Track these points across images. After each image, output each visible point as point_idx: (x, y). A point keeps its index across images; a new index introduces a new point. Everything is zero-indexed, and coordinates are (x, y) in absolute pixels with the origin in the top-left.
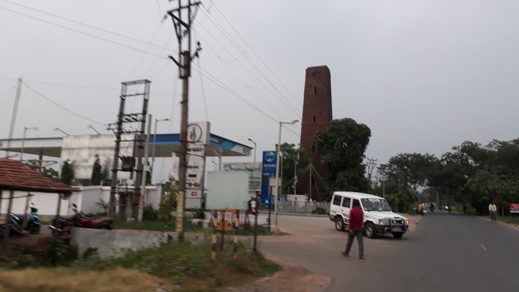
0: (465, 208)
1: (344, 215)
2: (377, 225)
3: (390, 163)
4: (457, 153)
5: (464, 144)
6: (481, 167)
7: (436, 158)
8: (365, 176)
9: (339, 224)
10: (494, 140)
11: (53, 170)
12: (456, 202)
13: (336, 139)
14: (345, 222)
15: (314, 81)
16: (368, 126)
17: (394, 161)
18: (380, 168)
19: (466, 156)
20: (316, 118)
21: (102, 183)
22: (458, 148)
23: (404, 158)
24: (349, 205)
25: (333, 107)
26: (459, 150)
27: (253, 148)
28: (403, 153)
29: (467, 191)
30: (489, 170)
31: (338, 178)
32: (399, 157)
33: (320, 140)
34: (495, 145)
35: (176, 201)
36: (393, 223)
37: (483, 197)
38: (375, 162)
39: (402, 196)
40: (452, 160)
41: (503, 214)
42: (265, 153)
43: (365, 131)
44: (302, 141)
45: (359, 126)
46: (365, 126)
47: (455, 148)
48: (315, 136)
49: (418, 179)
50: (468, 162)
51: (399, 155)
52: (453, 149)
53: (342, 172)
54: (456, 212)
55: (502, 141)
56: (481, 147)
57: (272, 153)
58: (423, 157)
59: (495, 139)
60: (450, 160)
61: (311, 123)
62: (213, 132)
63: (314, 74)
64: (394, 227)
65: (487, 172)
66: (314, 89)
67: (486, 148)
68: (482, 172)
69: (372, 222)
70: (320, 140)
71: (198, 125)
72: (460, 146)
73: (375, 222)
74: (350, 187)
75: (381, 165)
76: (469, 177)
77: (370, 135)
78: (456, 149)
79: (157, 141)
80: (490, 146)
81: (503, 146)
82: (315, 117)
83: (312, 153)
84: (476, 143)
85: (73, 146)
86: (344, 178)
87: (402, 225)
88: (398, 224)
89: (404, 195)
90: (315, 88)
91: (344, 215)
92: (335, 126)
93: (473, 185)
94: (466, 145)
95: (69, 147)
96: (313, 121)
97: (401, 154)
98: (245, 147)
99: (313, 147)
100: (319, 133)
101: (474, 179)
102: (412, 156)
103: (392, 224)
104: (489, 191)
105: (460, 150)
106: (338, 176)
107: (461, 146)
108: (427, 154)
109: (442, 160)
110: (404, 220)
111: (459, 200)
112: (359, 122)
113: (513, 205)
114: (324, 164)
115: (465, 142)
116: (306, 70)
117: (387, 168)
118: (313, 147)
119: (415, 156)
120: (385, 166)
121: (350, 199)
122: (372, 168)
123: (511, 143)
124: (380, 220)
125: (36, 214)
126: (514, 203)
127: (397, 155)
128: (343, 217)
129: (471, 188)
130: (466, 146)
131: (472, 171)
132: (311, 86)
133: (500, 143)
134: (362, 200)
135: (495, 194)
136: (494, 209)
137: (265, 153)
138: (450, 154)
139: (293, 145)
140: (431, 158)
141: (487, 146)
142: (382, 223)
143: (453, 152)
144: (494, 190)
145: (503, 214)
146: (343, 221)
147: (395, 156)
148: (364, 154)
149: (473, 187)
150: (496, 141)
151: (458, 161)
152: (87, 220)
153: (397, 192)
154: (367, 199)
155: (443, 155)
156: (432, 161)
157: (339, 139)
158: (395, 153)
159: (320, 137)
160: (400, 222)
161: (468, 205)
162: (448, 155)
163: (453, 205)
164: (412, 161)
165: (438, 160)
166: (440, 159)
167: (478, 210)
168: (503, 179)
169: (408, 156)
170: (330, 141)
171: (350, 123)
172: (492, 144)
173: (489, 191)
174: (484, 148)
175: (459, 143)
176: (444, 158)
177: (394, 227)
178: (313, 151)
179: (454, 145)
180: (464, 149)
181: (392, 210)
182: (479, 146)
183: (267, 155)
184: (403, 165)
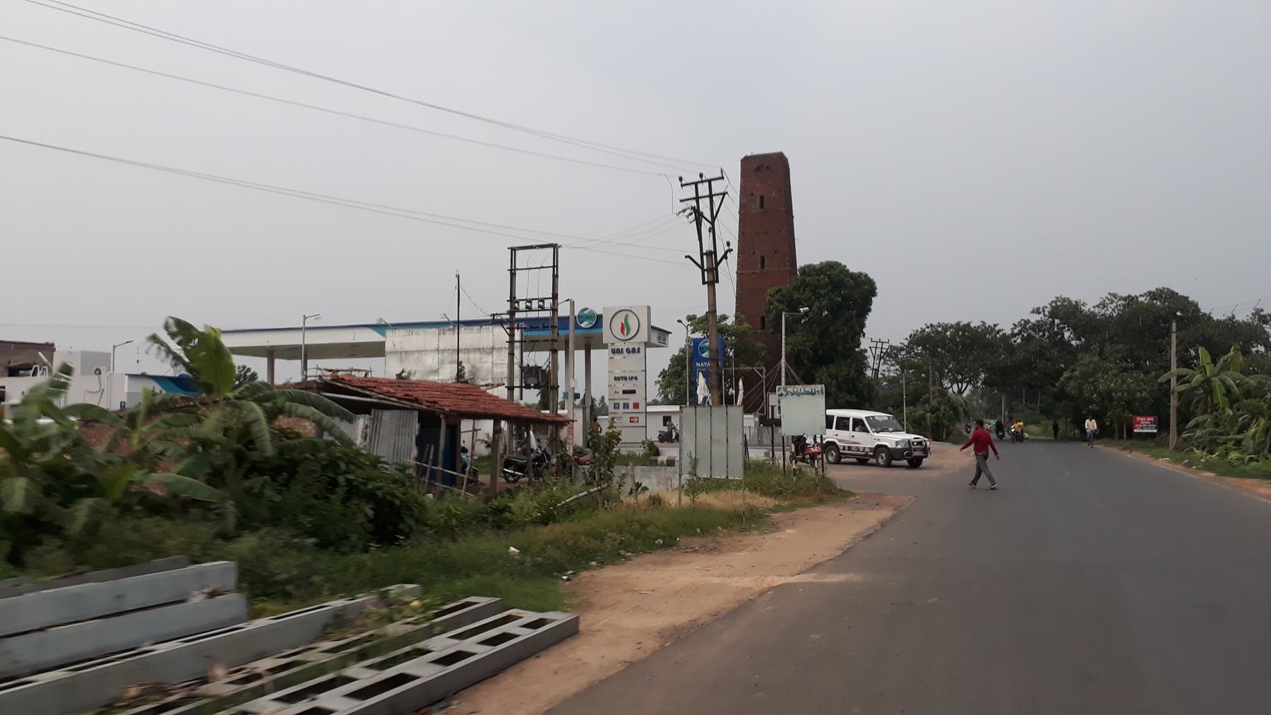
0: (1056, 428)
1: (840, 441)
2: (894, 449)
4: (1042, 321)
5: (1055, 302)
6: (1085, 348)
7: (1000, 331)
9: (832, 455)
10: (1110, 294)
12: (1043, 416)
14: (841, 451)
16: (871, 276)
19: (1058, 325)
24: (848, 426)
26: (1044, 314)
27: (671, 333)
28: (935, 323)
29: (1062, 395)
30: (1100, 355)
32: (927, 330)
34: (1112, 303)
35: (43, 435)
36: (914, 445)
39: (938, 409)
40: (1033, 333)
41: (1125, 436)
43: (866, 287)
44: (739, 308)
45: (852, 276)
46: (866, 276)
47: (1037, 311)
49: (963, 373)
50: (1063, 336)
52: (1033, 312)
54: (1043, 437)
55: (1125, 295)
56: (1085, 309)
58: (977, 328)
59: (1111, 292)
60: (1029, 334)
61: (757, 271)
62: (652, 324)
63: (758, 169)
64: (915, 450)
65: (1096, 359)
66: (758, 199)
67: (1097, 310)
68: (1087, 359)
69: (886, 446)
71: (616, 313)
72: (1046, 307)
73: (889, 446)
74: (841, 395)
77: (874, 294)
78: (1039, 313)
80: (1103, 305)
81: (1128, 304)
82: (763, 258)
83: (760, 331)
84: (1075, 302)
85: (407, 348)
87: (923, 447)
88: (919, 446)
90: (762, 198)
91: (840, 441)
92: (807, 279)
93: (1072, 383)
95: (398, 348)
97: (931, 325)
98: (661, 333)
99: (763, 319)
100: (777, 292)
103: (913, 447)
104: (1099, 394)
105: (1047, 313)
106: (817, 375)
107: (1049, 306)
108: (983, 322)
109: (1014, 335)
110: (925, 441)
111: (1047, 412)
112: (853, 268)
113: (1138, 419)
114: (790, 353)
115: (1056, 299)
116: (742, 161)
117: (903, 353)
118: (763, 319)
119: (958, 327)
121: (849, 419)
123: (1141, 299)
124: (897, 443)
125: (471, 447)
126: (1141, 415)
127: (924, 327)
128: (838, 443)
129: (1068, 390)
133: (1121, 298)
134: (867, 418)
135: (1111, 399)
136: (1094, 427)
138: (1028, 322)
140: (991, 330)
141: (1098, 306)
142: (899, 447)
143: (1034, 318)
144: (1109, 392)
145: (1125, 436)
146: (839, 449)
147: (920, 330)
149: (1071, 388)
150: (1115, 296)
151: (1044, 335)
152: (909, 426)
153: (927, 401)
154: (873, 417)
155: (1014, 325)
156: (992, 338)
160: (920, 443)
163: (1036, 423)
164: (953, 339)
165: (1004, 334)
166: (1008, 332)
168: (1125, 370)
169: (946, 328)
171: (836, 272)
172: (1107, 302)
173: (1099, 394)
174: (1092, 309)
175: (1045, 301)
176: (1016, 331)
177: (915, 450)
178: (763, 327)
179: (1036, 306)
180: (1054, 312)
182: (1083, 308)
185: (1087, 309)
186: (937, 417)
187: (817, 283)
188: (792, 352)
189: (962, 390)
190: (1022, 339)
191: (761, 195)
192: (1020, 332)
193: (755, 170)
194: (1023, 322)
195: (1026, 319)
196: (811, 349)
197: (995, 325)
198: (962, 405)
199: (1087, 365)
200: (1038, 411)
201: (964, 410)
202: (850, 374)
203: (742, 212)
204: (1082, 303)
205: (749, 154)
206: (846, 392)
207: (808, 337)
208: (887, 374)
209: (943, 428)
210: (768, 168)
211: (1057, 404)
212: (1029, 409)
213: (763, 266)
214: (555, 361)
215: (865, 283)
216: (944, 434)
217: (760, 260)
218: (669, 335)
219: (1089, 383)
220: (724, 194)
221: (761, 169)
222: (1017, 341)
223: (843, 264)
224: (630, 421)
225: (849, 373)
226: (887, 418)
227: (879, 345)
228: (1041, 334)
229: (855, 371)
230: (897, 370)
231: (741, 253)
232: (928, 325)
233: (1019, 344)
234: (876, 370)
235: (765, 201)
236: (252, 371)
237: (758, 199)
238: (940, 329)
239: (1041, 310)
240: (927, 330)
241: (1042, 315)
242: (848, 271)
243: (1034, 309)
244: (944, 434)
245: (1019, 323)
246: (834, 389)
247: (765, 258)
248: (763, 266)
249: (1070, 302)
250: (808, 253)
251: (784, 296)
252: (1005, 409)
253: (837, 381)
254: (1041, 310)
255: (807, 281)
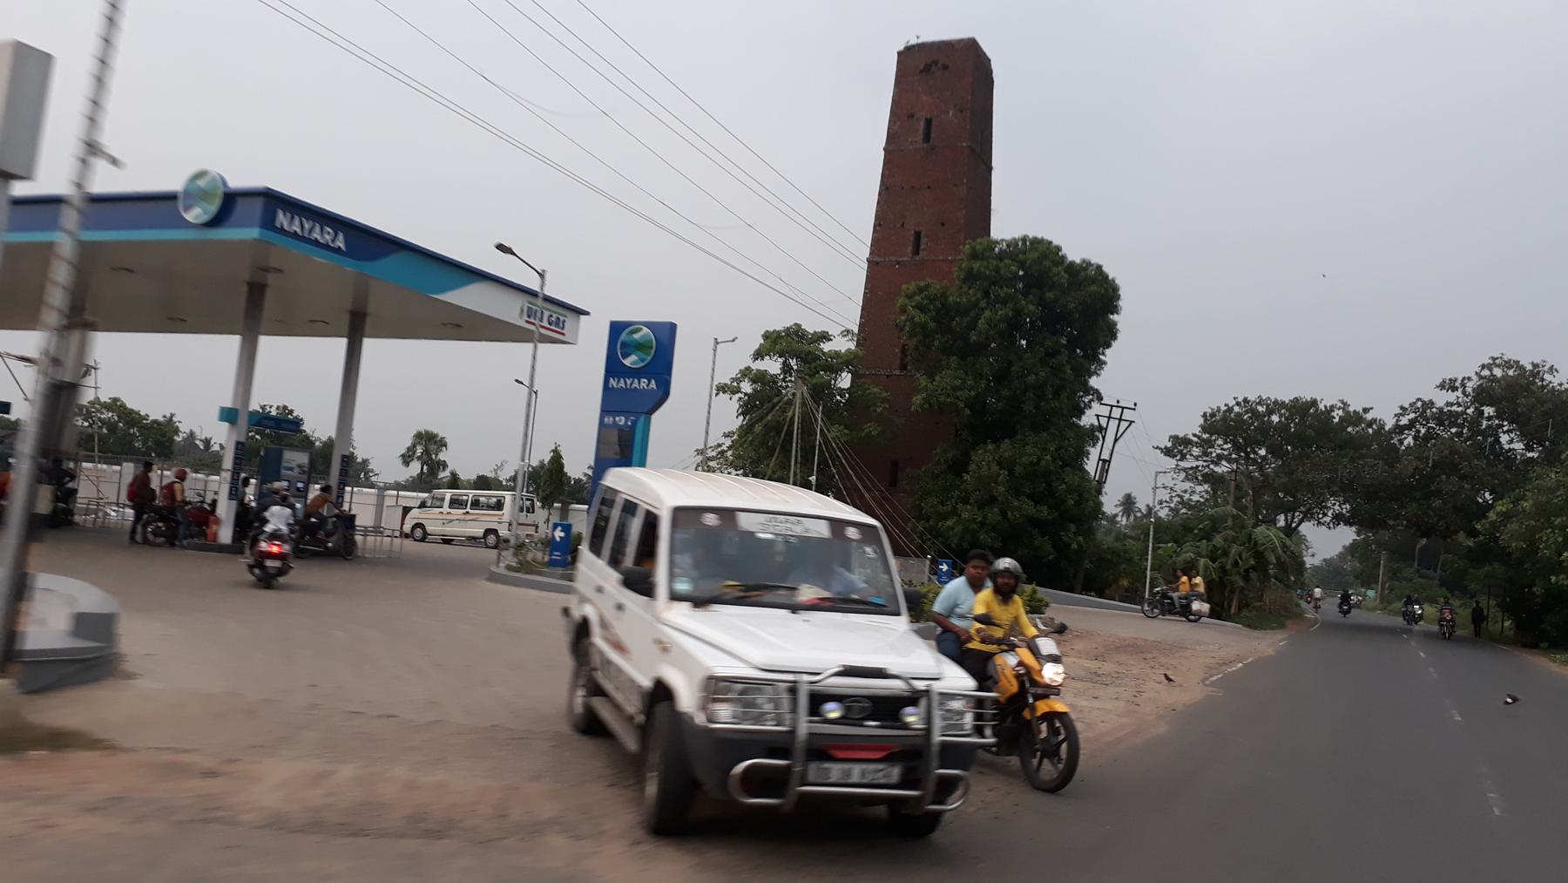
0: (1478, 617)
3: (1204, 429)
7: (1374, 421)
8: (1087, 467)
11: (123, 406)
13: (978, 317)
15: (925, 98)
16: (1111, 271)
17: (1221, 425)
18: (1166, 448)
19: (1489, 418)
20: (924, 241)
21: (1145, 564)
22: (1463, 385)
23: (1254, 412)
25: (993, 206)
26: (1464, 393)
27: (587, 313)
28: (1252, 397)
29: (1488, 552)
31: (972, 467)
32: (1237, 409)
33: (920, 317)
37: (1553, 579)
38: (1128, 415)
39: (1226, 553)
40: (1439, 430)
42: (617, 329)
43: (1093, 288)
46: (1099, 268)
48: (901, 301)
51: (1238, 404)
52: (1442, 386)
53: (990, 447)
57: (645, 330)
63: (927, 69)
64: (821, 750)
70: (920, 317)
72: (1469, 379)
75: (1175, 438)
76: (1498, 497)
78: (1454, 389)
79: (87, 225)
82: (918, 236)
86: (995, 468)
88: (872, 727)
89: (1234, 549)
90: (929, 122)
92: (976, 265)
93: (1513, 526)
94: (1498, 372)
96: (910, 249)
97: (1246, 400)
100: (921, 290)
101: (1516, 502)
102: (1314, 430)
105: (1469, 390)
107: (1475, 378)
109: (1399, 429)
111: (1455, 585)
112: (1074, 254)
116: (900, 54)
120: (1185, 442)
122: (1116, 440)
127: (1231, 403)
129: (1504, 537)
130: (1493, 378)
131: (1510, 474)
132: (911, 116)
137: (617, 329)
139: (825, 337)
140: (1354, 418)
143: (1442, 399)
148: (1094, 382)
149: (1511, 536)
151: (1460, 434)
154: (727, 514)
157: (987, 313)
158: (1222, 397)
159: (919, 307)
161: (1490, 605)
162: (1423, 409)
164: (1282, 428)
167: (1519, 626)
169: (1277, 406)
170: (958, 323)
175: (1467, 367)
176: (1404, 421)
180: (1483, 395)
181: (910, 609)
182: (1547, 377)
183: (624, 336)
184: (1253, 443)
185: (1556, 382)
186: (1223, 569)
187: (993, 273)
188: (927, 406)
189: (1294, 525)
190: (1415, 438)
191: (928, 116)
192: (1412, 423)
193: (921, 71)
194: (1419, 404)
195: (1426, 399)
196: (966, 406)
197: (1366, 410)
198: (1274, 550)
199: (1552, 491)
200: (1436, 582)
201: (1278, 559)
202: (1043, 463)
203: (891, 148)
204: (1548, 366)
205: (914, 41)
206: (1030, 497)
207: (964, 381)
208: (1187, 496)
209: (1232, 591)
210: (945, 67)
211: (1471, 570)
212: (1422, 577)
213: (916, 251)
214: (634, 423)
215: (1093, 281)
216: (1234, 604)
217: (912, 238)
218: (582, 317)
219: (1554, 528)
220: (1131, 422)
221: (933, 68)
222: (1406, 442)
223: (1056, 243)
224: (533, 512)
225: (1039, 459)
226: (822, 530)
227: (1116, 413)
228: (1453, 430)
229: (1054, 459)
230: (1207, 492)
231: (880, 225)
232: (1240, 400)
233: (1408, 447)
234: (1104, 461)
235: (934, 129)
236: (295, 414)
237: (922, 124)
238: (1260, 409)
239: (1457, 384)
240: (1237, 409)
241: (1459, 393)
242: (1064, 258)
243: (1444, 381)
244: (1234, 604)
245: (1411, 405)
246: (1001, 489)
247: (923, 233)
248: (916, 251)
249: (1521, 368)
250: (1006, 225)
251: (932, 300)
252: (1383, 574)
253: (1011, 472)
254: (1457, 384)
255: (975, 270)
